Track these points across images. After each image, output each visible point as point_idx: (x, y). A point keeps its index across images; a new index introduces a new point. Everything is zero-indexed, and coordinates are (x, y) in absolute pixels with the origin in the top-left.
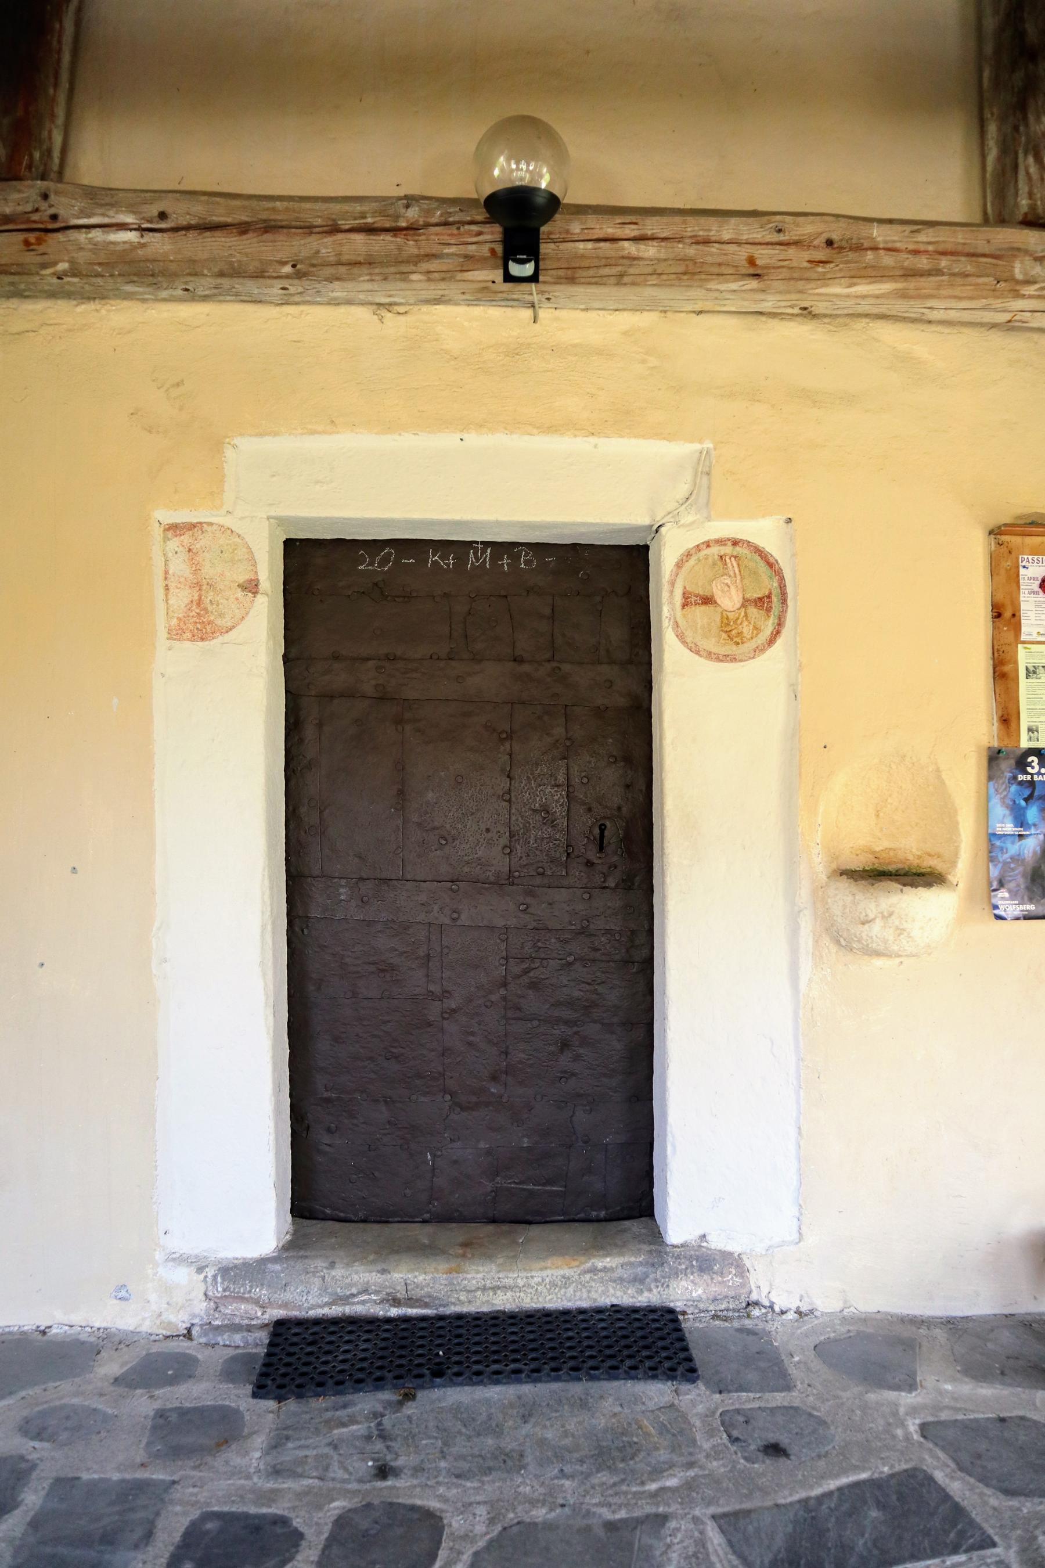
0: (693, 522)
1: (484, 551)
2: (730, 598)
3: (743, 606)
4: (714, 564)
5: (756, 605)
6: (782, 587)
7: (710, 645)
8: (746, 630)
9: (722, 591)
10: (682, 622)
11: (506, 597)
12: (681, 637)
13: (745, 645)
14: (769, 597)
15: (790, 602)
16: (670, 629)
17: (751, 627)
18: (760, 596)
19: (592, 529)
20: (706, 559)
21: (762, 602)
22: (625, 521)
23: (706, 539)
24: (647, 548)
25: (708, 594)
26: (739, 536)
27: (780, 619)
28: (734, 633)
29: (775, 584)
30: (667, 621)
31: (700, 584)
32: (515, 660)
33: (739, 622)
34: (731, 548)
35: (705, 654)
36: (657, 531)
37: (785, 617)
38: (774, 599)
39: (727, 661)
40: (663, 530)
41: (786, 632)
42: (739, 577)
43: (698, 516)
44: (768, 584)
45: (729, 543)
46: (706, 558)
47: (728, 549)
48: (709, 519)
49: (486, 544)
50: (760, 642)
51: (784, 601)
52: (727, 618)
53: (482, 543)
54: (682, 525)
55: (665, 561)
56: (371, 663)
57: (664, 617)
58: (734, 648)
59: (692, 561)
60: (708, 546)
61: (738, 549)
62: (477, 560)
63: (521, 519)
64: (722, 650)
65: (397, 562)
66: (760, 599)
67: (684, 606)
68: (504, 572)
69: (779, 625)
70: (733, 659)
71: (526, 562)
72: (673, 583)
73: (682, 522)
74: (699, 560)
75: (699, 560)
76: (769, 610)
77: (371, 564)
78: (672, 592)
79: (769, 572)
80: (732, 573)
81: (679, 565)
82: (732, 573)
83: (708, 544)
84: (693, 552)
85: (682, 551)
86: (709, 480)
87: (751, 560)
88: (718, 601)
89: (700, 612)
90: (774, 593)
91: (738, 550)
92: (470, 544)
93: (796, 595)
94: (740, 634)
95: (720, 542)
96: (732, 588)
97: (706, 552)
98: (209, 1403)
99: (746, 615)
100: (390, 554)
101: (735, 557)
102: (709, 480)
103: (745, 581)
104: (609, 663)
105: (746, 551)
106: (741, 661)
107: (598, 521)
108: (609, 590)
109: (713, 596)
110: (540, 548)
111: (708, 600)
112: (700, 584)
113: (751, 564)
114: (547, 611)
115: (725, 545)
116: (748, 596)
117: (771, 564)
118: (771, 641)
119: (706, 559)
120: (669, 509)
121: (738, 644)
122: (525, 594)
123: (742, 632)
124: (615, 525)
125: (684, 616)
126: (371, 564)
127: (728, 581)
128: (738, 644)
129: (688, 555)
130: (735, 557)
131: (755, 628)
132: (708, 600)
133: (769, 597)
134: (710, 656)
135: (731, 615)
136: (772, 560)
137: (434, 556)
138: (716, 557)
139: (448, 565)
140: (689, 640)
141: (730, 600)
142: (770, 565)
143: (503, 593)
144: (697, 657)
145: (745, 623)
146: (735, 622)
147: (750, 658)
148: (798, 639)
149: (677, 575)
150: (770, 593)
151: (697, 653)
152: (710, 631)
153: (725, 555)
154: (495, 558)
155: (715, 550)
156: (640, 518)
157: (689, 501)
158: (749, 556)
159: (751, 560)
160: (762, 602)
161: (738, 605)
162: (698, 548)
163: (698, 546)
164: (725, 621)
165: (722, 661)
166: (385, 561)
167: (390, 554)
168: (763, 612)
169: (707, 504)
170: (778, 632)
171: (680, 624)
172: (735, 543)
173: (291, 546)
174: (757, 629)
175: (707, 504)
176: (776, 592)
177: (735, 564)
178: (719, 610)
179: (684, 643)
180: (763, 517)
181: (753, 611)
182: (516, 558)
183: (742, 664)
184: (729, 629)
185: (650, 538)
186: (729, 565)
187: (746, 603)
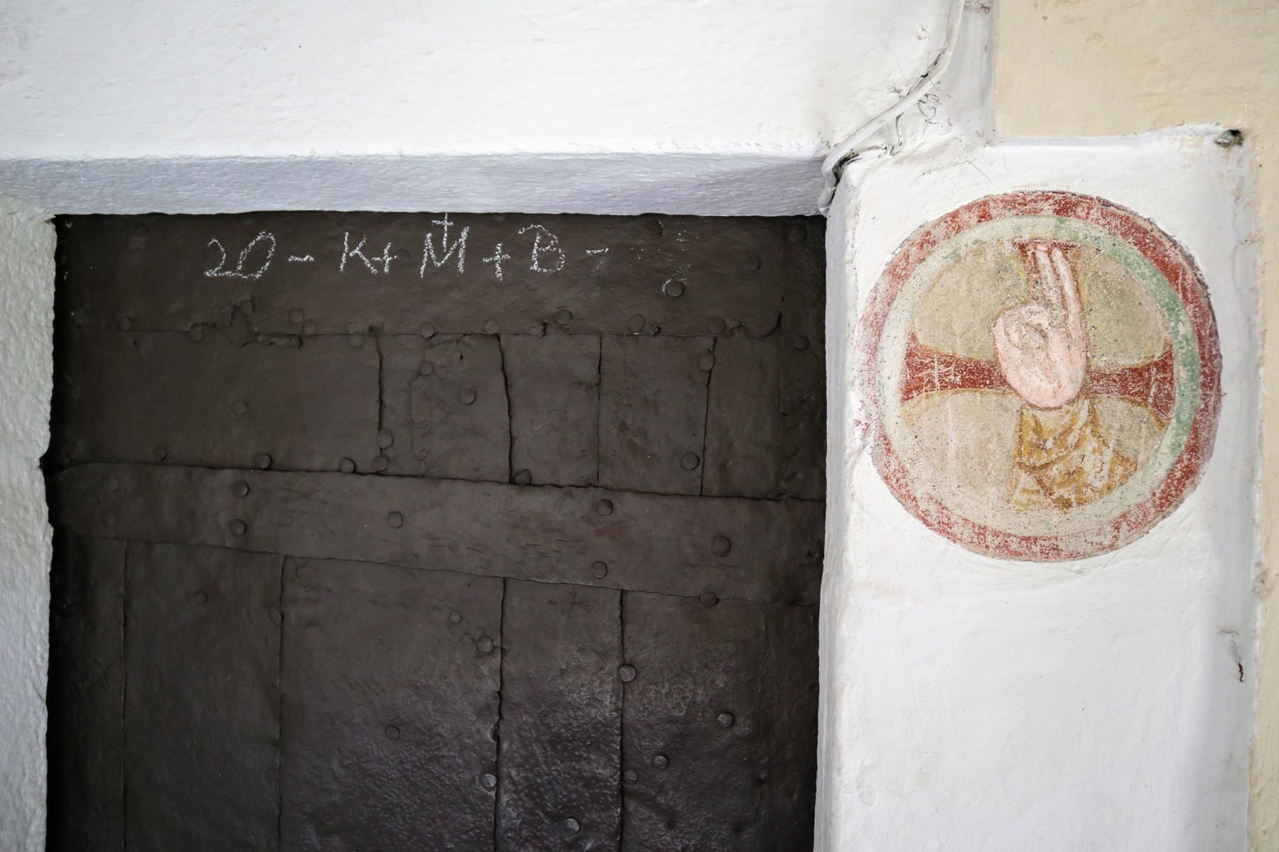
0: (940, 149)
1: (454, 236)
2: (1048, 369)
3: (1086, 392)
4: (1002, 268)
5: (1124, 390)
6: (1206, 336)
7: (983, 506)
8: (1094, 463)
9: (1024, 348)
10: (901, 440)
11: (497, 336)
12: (897, 482)
13: (1089, 508)
14: (1164, 365)
15: (1229, 383)
16: (866, 458)
17: (1108, 455)
18: (1137, 362)
19: (666, 175)
20: (978, 253)
21: (1144, 383)
22: (742, 149)
23: (978, 196)
24: (819, 223)
25: (982, 357)
26: (1077, 188)
27: (1195, 431)
28: (1054, 472)
29: (1185, 329)
30: (858, 432)
31: (958, 327)
32: (512, 481)
33: (1072, 439)
34: (1053, 221)
35: (967, 533)
36: (837, 176)
37: (1212, 428)
38: (1181, 373)
39: (1032, 557)
40: (851, 170)
41: (1212, 472)
42: (1074, 308)
43: (956, 131)
44: (1161, 328)
45: (1048, 208)
46: (979, 249)
47: (1044, 226)
48: (988, 137)
49: (460, 219)
50: (1132, 500)
51: (1210, 378)
52: (1038, 429)
53: (454, 216)
54: (911, 158)
55: (859, 261)
56: (228, 475)
57: (850, 422)
58: (1055, 515)
59: (936, 262)
60: (985, 217)
61: (1073, 224)
62: (440, 253)
63: (473, 149)
64: (1019, 525)
65: (279, 260)
66: (1137, 372)
67: (909, 391)
68: (495, 282)
69: (1193, 449)
70: (1051, 551)
71: (545, 260)
72: (877, 325)
73: (908, 148)
74: (957, 258)
75: (957, 258)
76: (1162, 406)
77: (230, 265)
78: (874, 350)
79: (1166, 291)
80: (1053, 296)
81: (898, 272)
82: (1053, 296)
83: (983, 211)
84: (939, 233)
85: (908, 229)
86: (991, 27)
87: (1114, 256)
88: (1012, 378)
89: (956, 412)
90: (1179, 353)
91: (1075, 227)
92: (425, 219)
93: (1253, 363)
94: (1072, 475)
95: (1020, 204)
96: (1056, 341)
97: (983, 232)
98: (849, 357)
99: (1093, 420)
100: (267, 243)
101: (1065, 248)
102: (991, 27)
103: (1094, 319)
104: (724, 497)
105: (1097, 231)
106: (1074, 556)
107: (668, 148)
108: (731, 324)
109: (994, 364)
110: (572, 226)
111: (980, 375)
112: (958, 327)
113: (1113, 270)
114: (586, 370)
115: (1036, 212)
116: (1100, 363)
117: (1172, 268)
118: (1168, 497)
119: (978, 253)
120: (871, 112)
121: (1066, 504)
122: (538, 330)
123: (1080, 471)
124: (718, 159)
125: (909, 419)
126: (230, 265)
127: (1043, 320)
128: (1066, 504)
129: (926, 241)
130: (1065, 248)
131: (1120, 457)
132: (980, 375)
133: (1164, 365)
134: (984, 539)
135: (1050, 422)
136: (1174, 257)
137: (352, 248)
138: (1008, 248)
139: (380, 266)
140: (919, 491)
141: (1045, 374)
142: (1170, 272)
143: (491, 329)
144: (942, 542)
145: (1091, 444)
146: (1061, 438)
147: (1103, 548)
148: (1258, 499)
149: (891, 300)
150: (1169, 355)
151: (944, 528)
152: (984, 465)
153: (1035, 242)
154: (478, 249)
155: (1005, 228)
156: (792, 142)
157: (928, 87)
158: (1106, 246)
159: (1114, 256)
160: (1144, 383)
161: (1070, 391)
162: (953, 222)
163: (954, 215)
164: (1031, 437)
165: (1016, 555)
166: (254, 262)
167: (267, 243)
168: (1144, 412)
169: (983, 94)
170: (1190, 472)
171: (895, 445)
172: (1066, 206)
173: (71, 231)
174: (1126, 463)
175: (983, 94)
176: (1185, 350)
177: (1063, 269)
178: (1013, 402)
179: (907, 499)
180: (1155, 127)
181: (1115, 408)
182: (520, 250)
183: (1078, 564)
184: (1039, 459)
185: (823, 198)
186: (1047, 272)
187: (1094, 382)
